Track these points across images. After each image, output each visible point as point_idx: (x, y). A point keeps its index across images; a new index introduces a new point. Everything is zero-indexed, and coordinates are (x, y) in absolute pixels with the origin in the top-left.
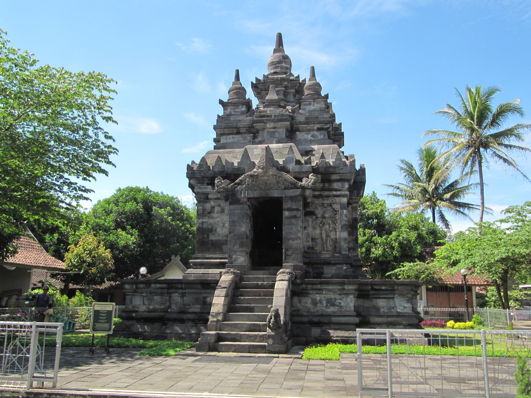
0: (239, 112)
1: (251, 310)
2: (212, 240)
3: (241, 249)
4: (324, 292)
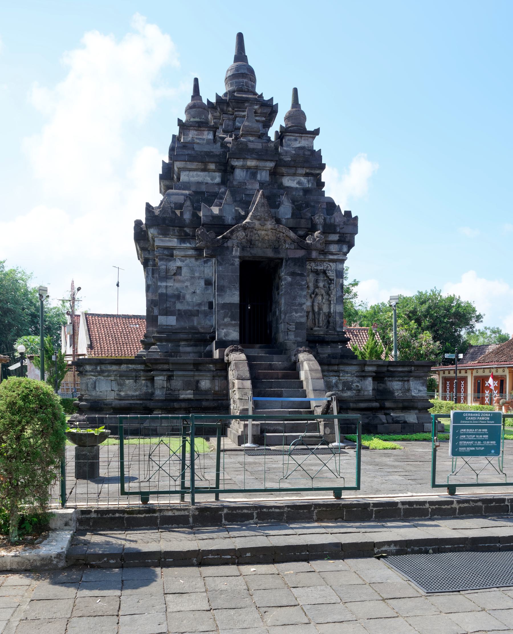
0: (204, 139)
1: (280, 395)
2: (179, 310)
3: (233, 322)
4: (341, 374)
